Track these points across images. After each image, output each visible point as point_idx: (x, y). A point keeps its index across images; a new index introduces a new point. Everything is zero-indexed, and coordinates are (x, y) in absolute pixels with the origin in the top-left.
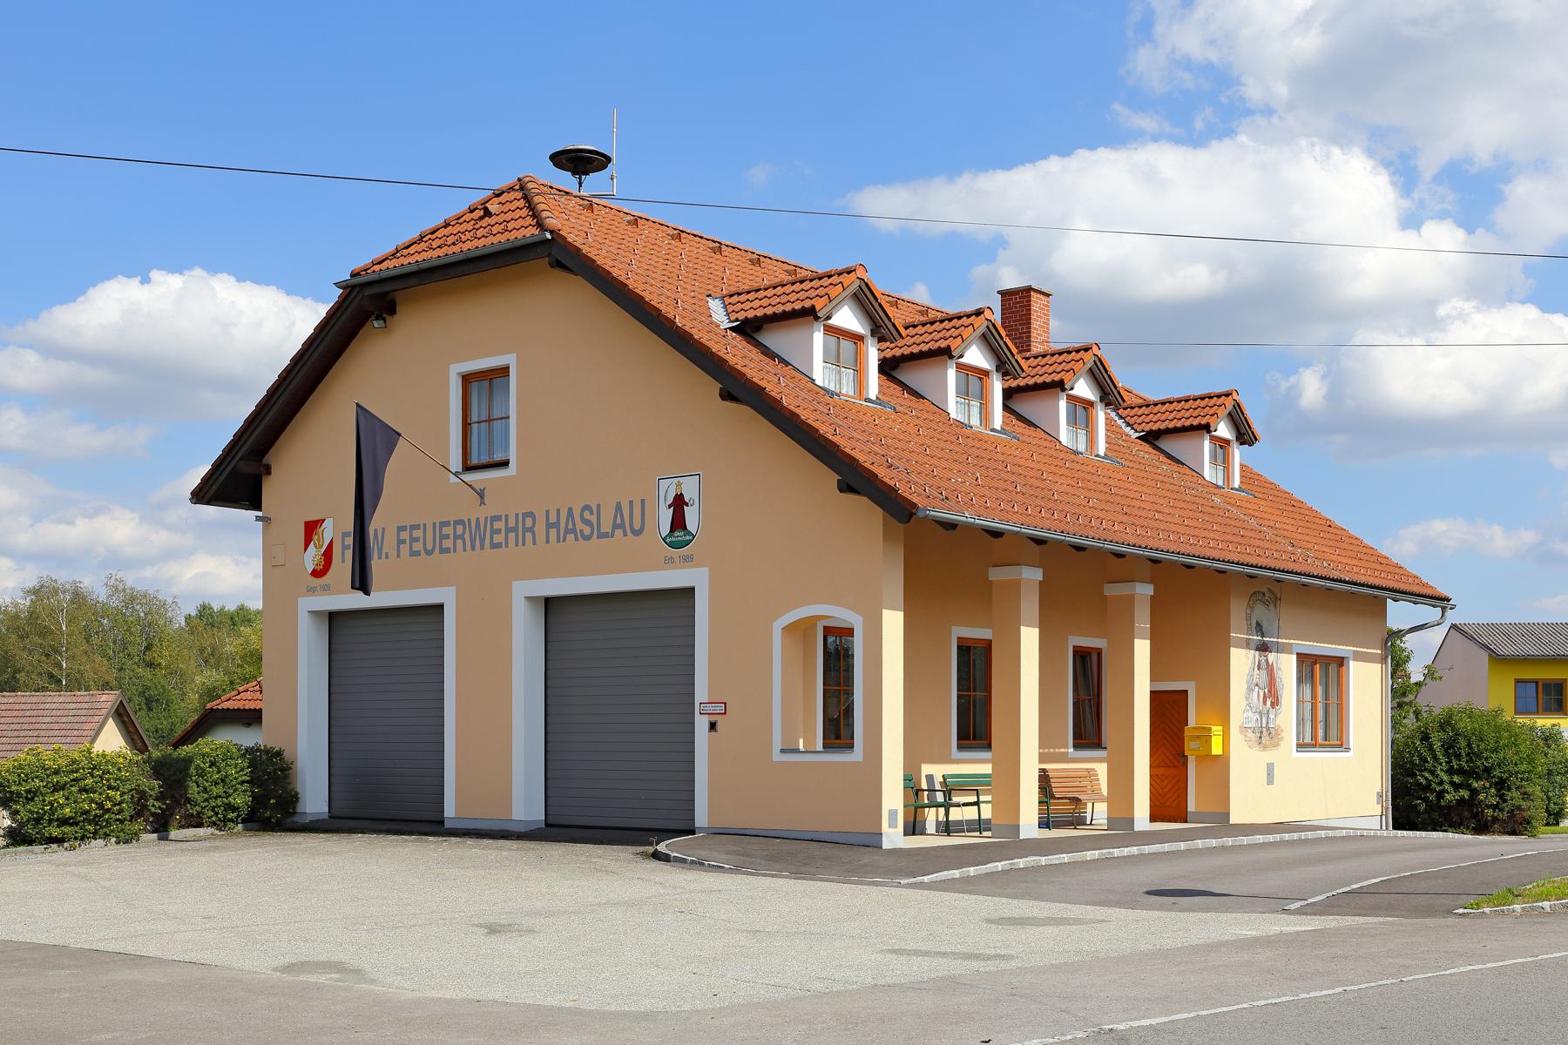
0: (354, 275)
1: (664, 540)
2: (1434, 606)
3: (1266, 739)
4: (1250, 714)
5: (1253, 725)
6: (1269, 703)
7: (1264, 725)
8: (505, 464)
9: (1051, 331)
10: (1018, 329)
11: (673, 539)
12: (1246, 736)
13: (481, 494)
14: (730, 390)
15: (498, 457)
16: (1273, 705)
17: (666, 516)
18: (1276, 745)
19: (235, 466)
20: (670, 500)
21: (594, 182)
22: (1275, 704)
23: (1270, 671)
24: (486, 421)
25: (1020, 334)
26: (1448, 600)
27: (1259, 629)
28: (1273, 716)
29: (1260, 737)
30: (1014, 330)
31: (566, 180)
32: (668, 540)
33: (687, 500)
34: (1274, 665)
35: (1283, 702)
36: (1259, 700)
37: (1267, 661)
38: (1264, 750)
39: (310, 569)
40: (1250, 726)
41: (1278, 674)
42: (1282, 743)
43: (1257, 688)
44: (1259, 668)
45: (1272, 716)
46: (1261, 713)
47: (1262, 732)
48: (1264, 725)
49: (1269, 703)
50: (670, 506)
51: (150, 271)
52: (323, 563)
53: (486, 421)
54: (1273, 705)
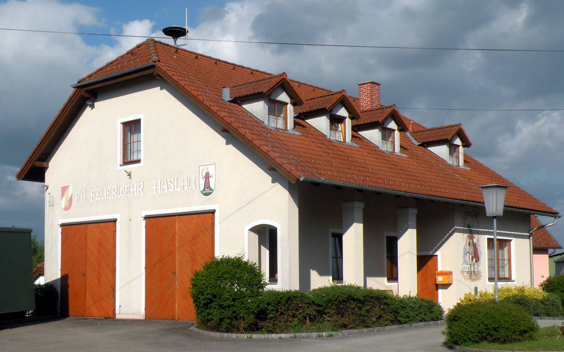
0: (79, 82)
1: (202, 192)
2: (552, 217)
3: (473, 277)
4: (465, 265)
5: (467, 270)
6: (474, 260)
7: (472, 270)
8: (138, 161)
9: (380, 92)
10: (364, 96)
11: (205, 192)
12: (463, 275)
13: (129, 175)
14: (452, 285)
15: (135, 158)
16: (476, 261)
17: (202, 182)
18: (478, 279)
19: (33, 164)
20: (204, 175)
21: (180, 41)
22: (477, 261)
23: (475, 246)
24: (135, 142)
25: (367, 94)
26: (558, 214)
27: (469, 226)
28: (477, 266)
29: (471, 276)
30: (362, 95)
31: (169, 40)
32: (203, 192)
33: (210, 175)
34: (477, 244)
35: (481, 260)
36: (469, 259)
37: (473, 242)
38: (473, 281)
39: (63, 206)
40: (465, 270)
41: (478, 248)
42: (482, 278)
43: (468, 254)
44: (469, 245)
45: (476, 266)
46: (471, 265)
47: (471, 273)
48: (472, 270)
49: (474, 260)
50: (204, 178)
51: (365, 204)
52: (68, 204)
53: (135, 142)
54: (476, 261)
